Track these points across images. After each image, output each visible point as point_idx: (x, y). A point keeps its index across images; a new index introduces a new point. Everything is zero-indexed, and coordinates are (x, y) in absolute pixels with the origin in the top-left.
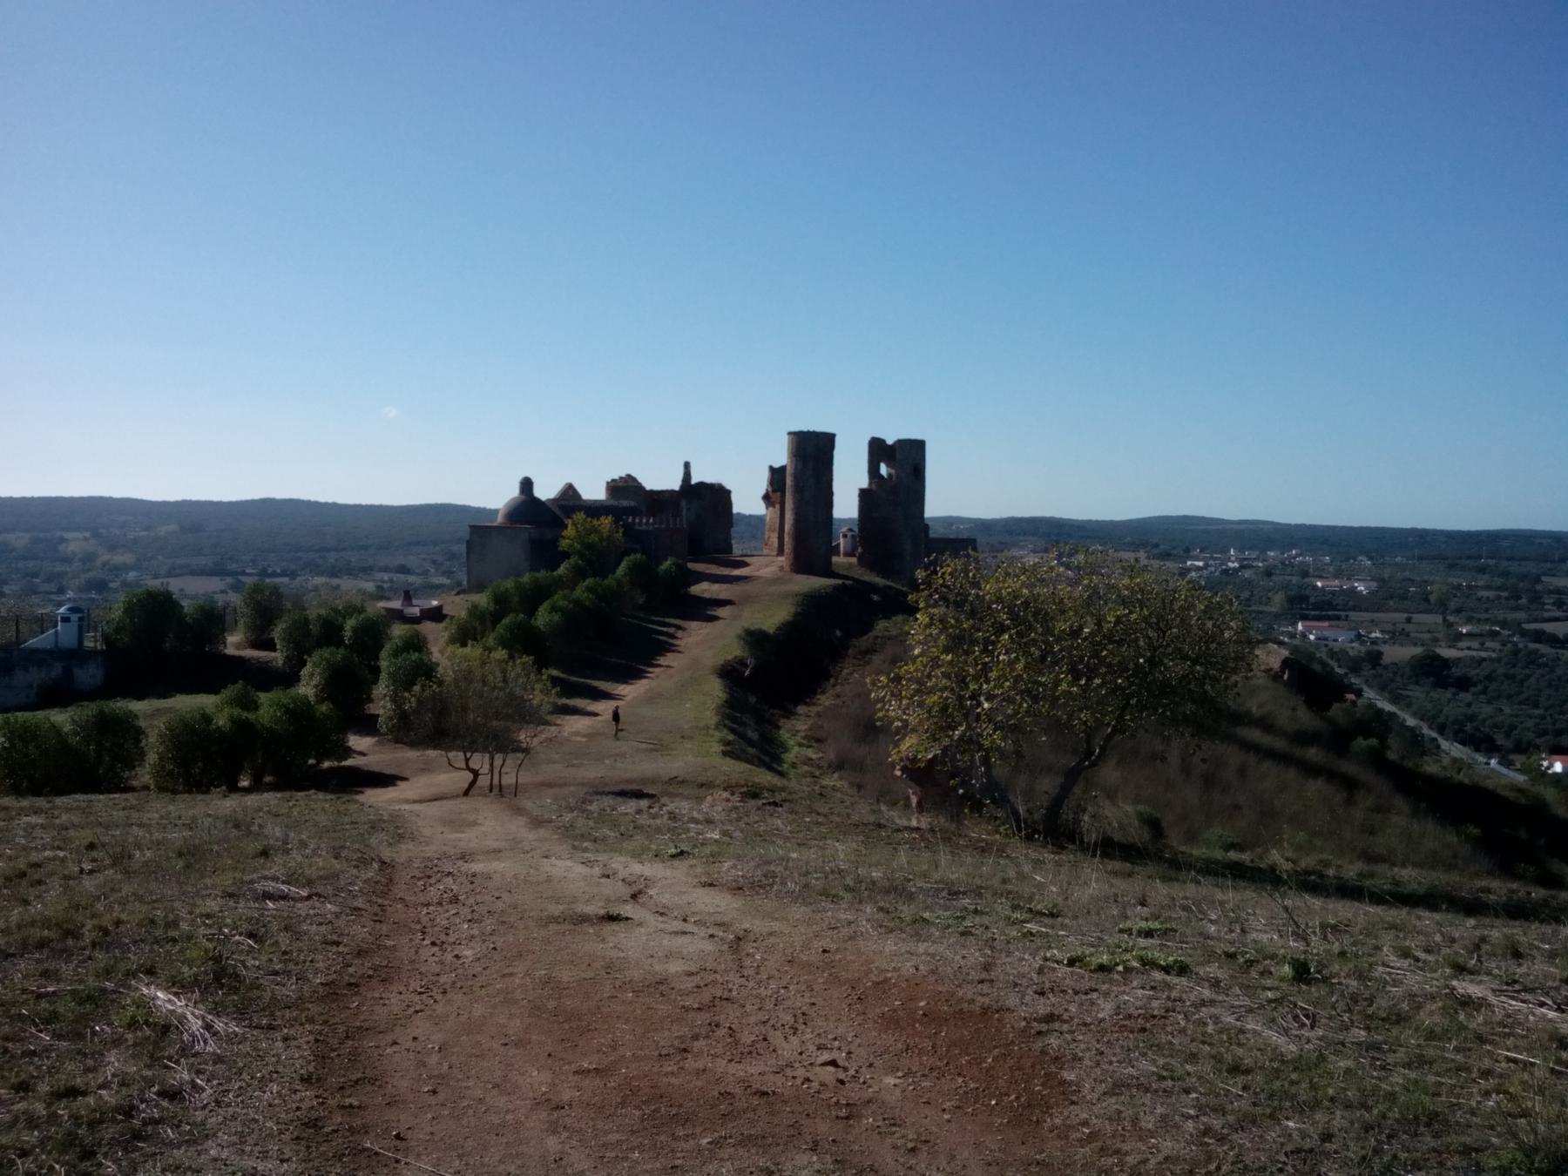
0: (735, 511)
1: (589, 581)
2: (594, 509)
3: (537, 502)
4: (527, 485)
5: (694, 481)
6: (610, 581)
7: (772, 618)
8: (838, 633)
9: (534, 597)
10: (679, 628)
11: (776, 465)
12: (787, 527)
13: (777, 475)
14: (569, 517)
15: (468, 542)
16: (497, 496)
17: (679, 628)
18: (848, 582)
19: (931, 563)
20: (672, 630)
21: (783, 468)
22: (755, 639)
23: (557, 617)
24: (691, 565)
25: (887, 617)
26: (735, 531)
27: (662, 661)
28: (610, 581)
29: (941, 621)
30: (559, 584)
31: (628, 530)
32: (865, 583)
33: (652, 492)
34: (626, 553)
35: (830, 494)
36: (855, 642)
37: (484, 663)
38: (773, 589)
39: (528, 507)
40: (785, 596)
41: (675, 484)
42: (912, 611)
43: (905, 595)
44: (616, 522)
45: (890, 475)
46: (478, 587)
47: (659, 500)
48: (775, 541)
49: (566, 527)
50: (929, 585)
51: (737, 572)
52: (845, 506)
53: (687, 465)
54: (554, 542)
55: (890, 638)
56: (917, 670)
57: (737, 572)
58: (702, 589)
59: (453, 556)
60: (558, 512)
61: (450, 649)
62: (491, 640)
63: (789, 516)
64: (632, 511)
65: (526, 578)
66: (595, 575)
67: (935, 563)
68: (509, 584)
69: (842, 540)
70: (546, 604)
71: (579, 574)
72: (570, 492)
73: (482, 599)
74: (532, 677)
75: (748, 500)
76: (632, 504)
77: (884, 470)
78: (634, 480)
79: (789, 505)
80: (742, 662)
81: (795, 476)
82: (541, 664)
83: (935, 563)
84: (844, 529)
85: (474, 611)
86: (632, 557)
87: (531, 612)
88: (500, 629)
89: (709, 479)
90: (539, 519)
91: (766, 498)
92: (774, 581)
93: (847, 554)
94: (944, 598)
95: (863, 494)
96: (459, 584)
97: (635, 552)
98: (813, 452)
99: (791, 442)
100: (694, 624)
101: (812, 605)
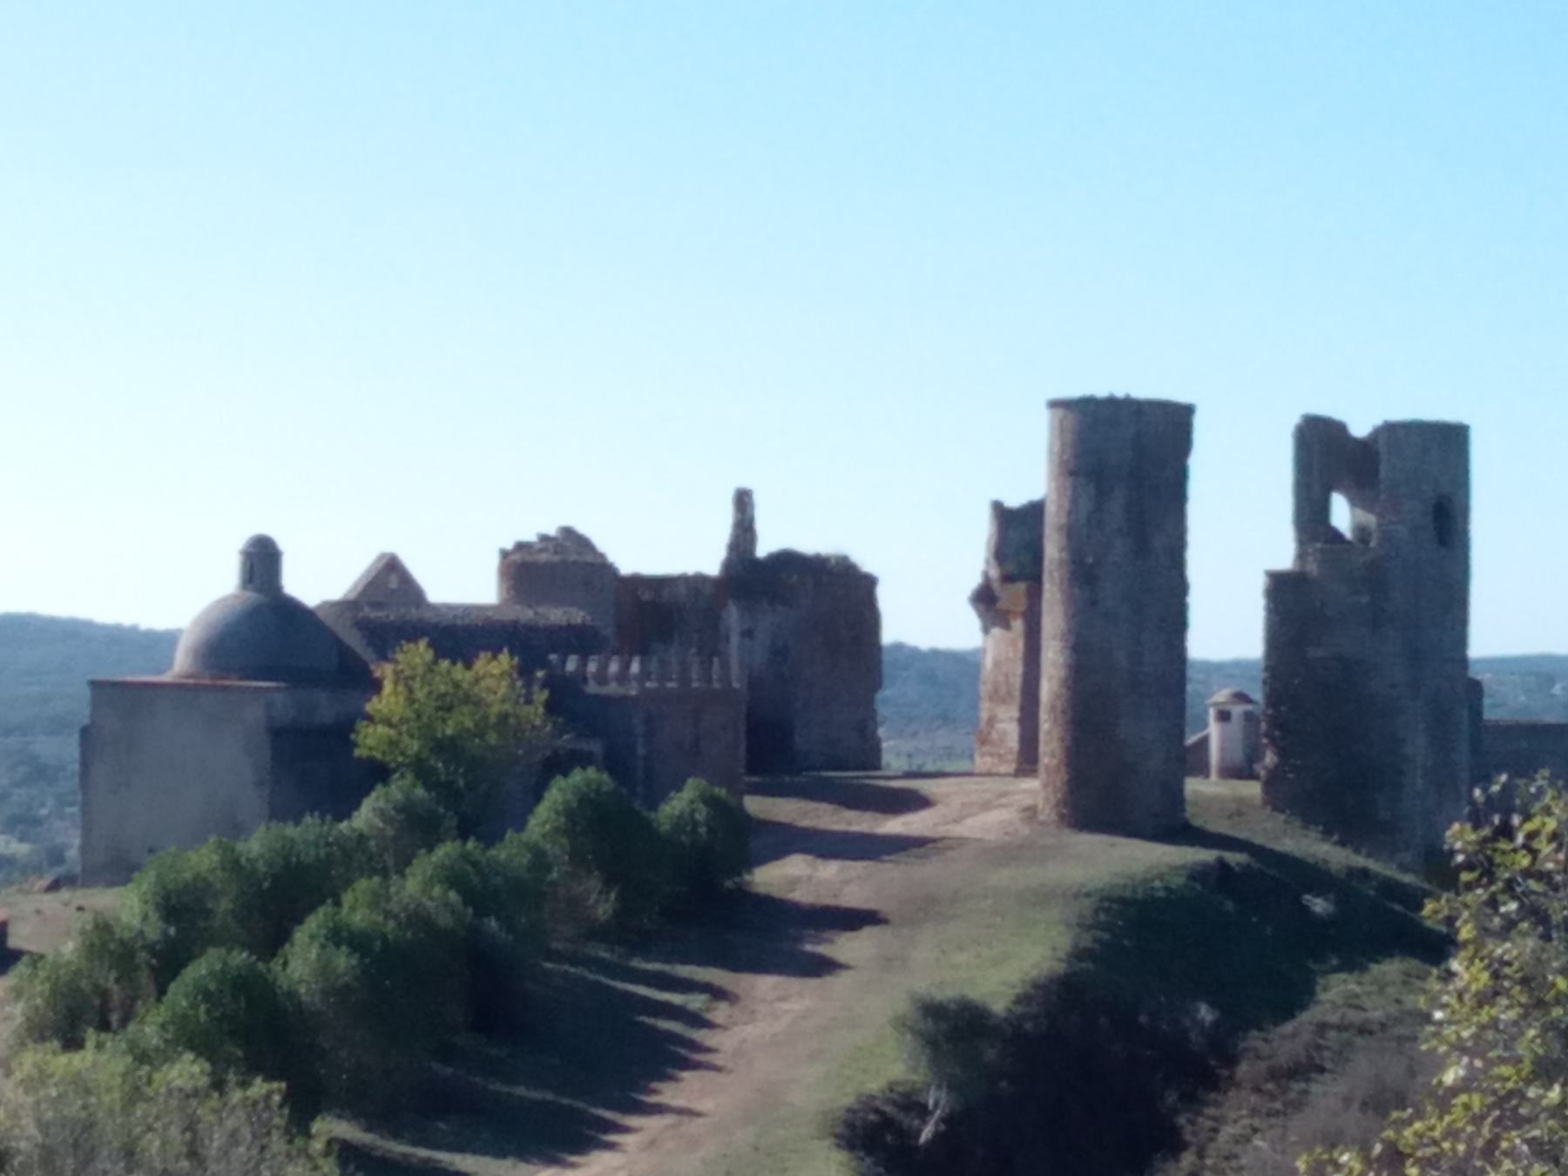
0: (890, 633)
1: (446, 851)
2: (459, 636)
3: (291, 611)
4: (262, 560)
5: (765, 547)
6: (510, 852)
7: (1004, 964)
8: (1205, 1013)
9: (280, 900)
10: (718, 994)
11: (1015, 499)
12: (1050, 687)
13: (1016, 530)
14: (384, 657)
15: (85, 733)
16: (173, 594)
17: (718, 994)
18: (1235, 858)
19: (1492, 804)
20: (695, 1002)
21: (1035, 511)
22: (952, 1028)
23: (343, 961)
24: (755, 805)
25: (1351, 965)
26: (889, 700)
27: (668, 1094)
28: (510, 852)
29: (1525, 982)
30: (356, 858)
31: (566, 700)
32: (1283, 860)
33: (637, 581)
34: (558, 765)
35: (1177, 588)
36: (1254, 1040)
37: (135, 1095)
38: (1002, 877)
39: (268, 633)
40: (1043, 897)
41: (704, 556)
42: (1435, 948)
43: (1414, 900)
44: (525, 671)
45: (1362, 532)
46: (118, 870)
47: (655, 612)
48: (1009, 728)
49: (376, 686)
50: (1488, 872)
51: (894, 825)
52: (1226, 624)
53: (743, 501)
54: (341, 733)
55: (1364, 1030)
56: (1452, 1134)
57: (894, 825)
58: (788, 877)
59: (40, 772)
60: (355, 641)
61: (29, 1060)
62: (150, 1028)
63: (1053, 657)
64: (581, 640)
65: (256, 845)
66: (464, 835)
67: (1503, 804)
68: (203, 859)
69: (1214, 730)
70: (314, 923)
71: (418, 828)
72: (390, 580)
73: (128, 906)
74: (277, 1143)
75: (929, 604)
76: (578, 616)
77: (1342, 514)
78: (584, 543)
79: (1053, 620)
80: (913, 1105)
81: (1071, 533)
82: (303, 1107)
83: (1503, 804)
84: (1222, 695)
85: (105, 943)
86: (577, 777)
87: (273, 941)
88: (179, 992)
89: (810, 543)
90: (298, 669)
91: (985, 599)
92: (1005, 853)
93: (1232, 772)
94: (1539, 916)
95: (1281, 588)
96: (56, 857)
97: (584, 760)
98: (1128, 461)
99: (1060, 430)
100: (766, 984)
101: (1132, 931)
